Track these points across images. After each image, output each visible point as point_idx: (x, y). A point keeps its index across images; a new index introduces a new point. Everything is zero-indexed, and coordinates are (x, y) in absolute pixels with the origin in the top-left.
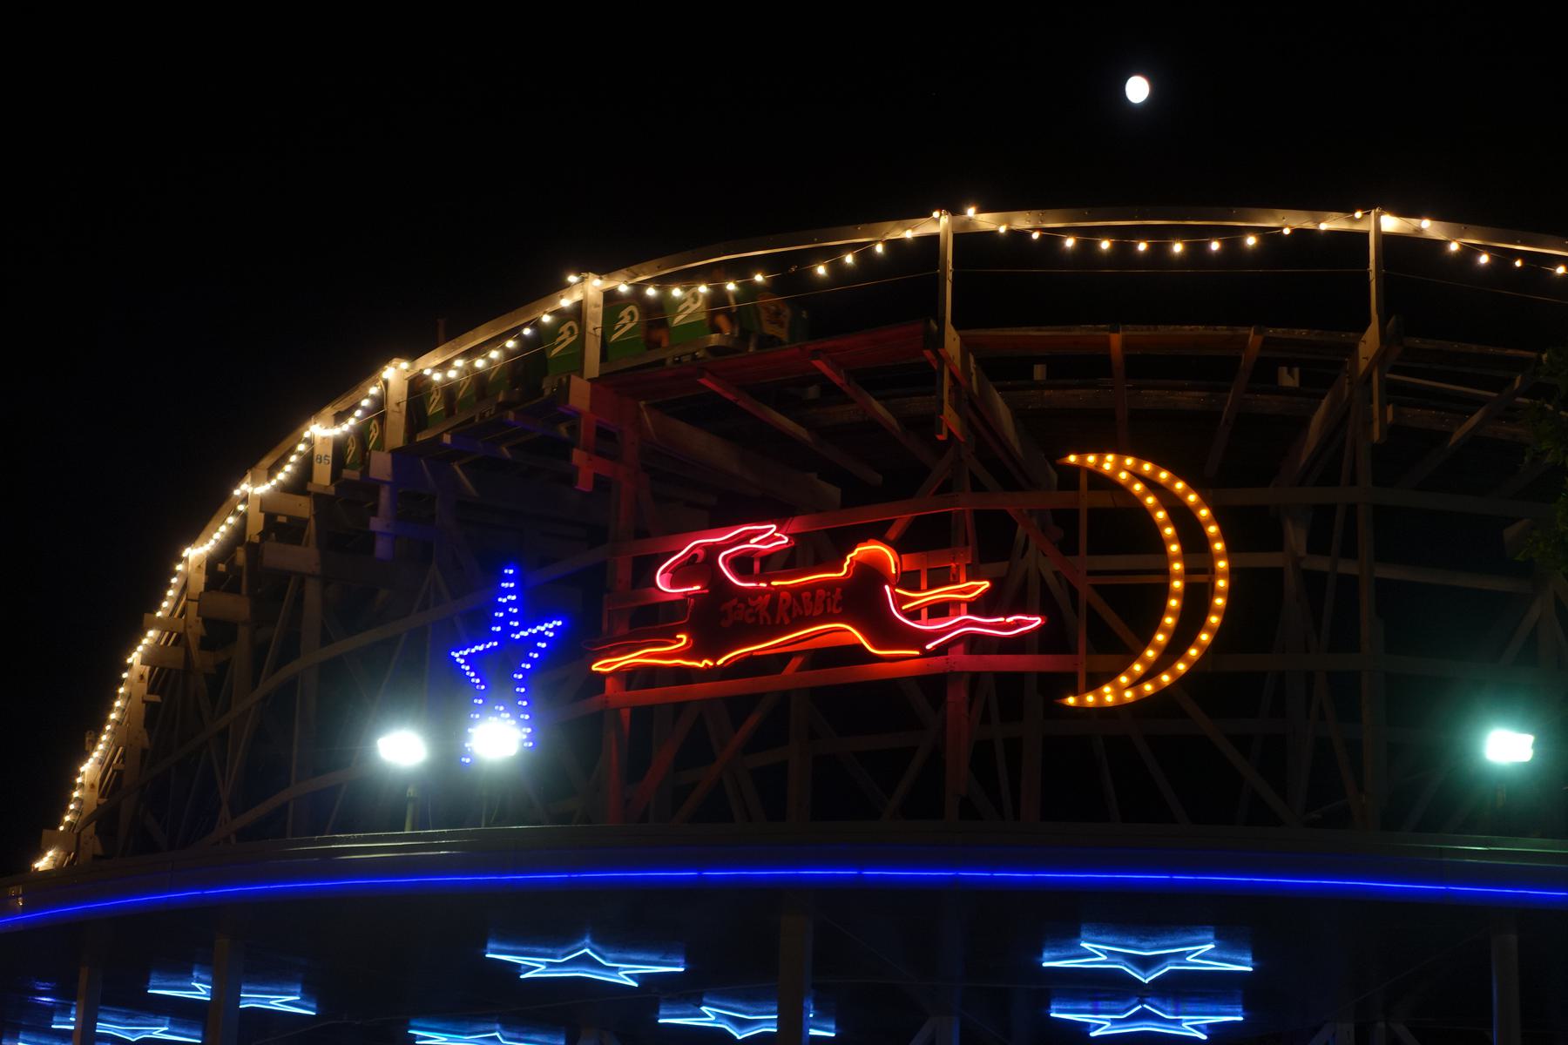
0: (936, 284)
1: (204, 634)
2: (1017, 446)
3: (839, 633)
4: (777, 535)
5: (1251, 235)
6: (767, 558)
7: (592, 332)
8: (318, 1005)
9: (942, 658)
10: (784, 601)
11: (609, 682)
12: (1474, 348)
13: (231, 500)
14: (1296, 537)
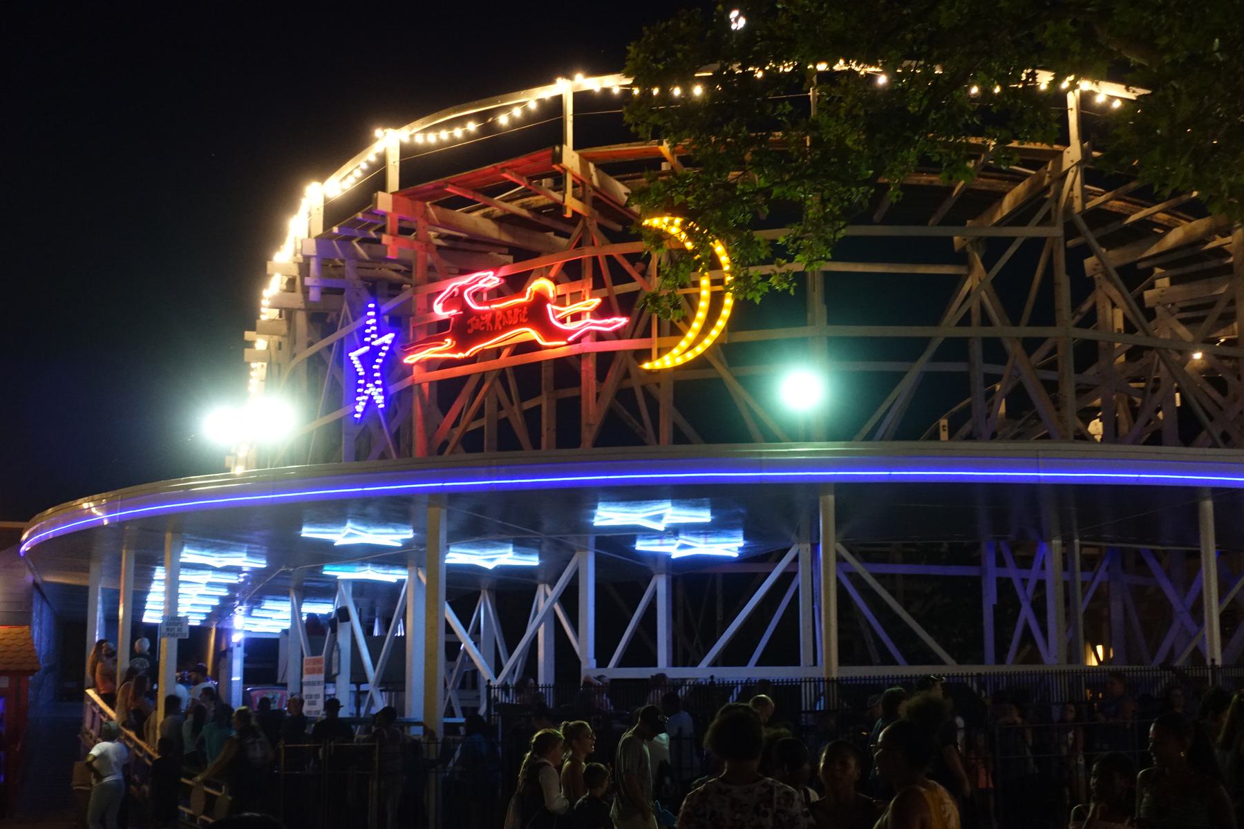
0: (561, 125)
5: (376, 128)
8: (267, 561)
11: (415, 368)
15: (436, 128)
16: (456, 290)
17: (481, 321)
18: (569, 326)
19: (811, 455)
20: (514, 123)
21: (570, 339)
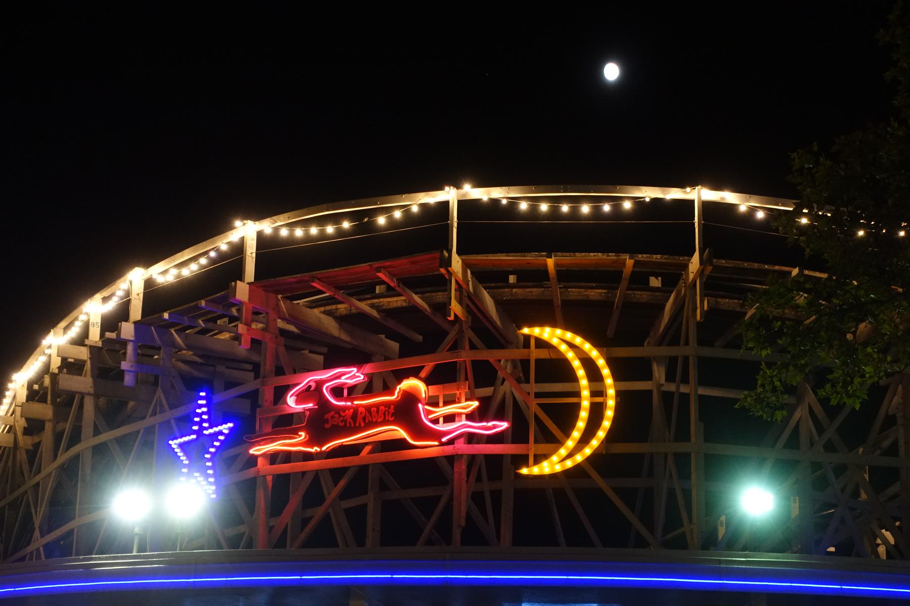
0: (447, 229)
1: (26, 426)
2: (498, 322)
3: (393, 432)
4: (357, 374)
6: (352, 389)
7: (250, 255)
9: (451, 447)
10: (361, 413)
11: (260, 460)
12: (756, 265)
13: (42, 346)
14: (659, 373)
15: (305, 223)
16: (313, 384)
17: (340, 416)
18: (441, 427)
19: (767, 566)
20: (392, 223)
21: (444, 440)
